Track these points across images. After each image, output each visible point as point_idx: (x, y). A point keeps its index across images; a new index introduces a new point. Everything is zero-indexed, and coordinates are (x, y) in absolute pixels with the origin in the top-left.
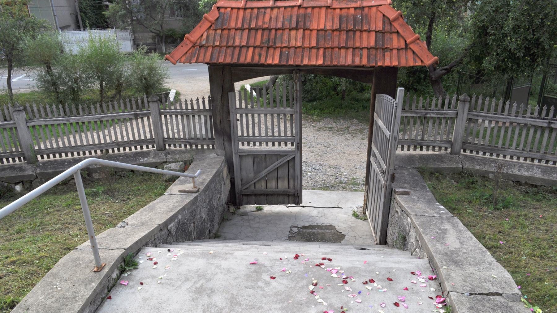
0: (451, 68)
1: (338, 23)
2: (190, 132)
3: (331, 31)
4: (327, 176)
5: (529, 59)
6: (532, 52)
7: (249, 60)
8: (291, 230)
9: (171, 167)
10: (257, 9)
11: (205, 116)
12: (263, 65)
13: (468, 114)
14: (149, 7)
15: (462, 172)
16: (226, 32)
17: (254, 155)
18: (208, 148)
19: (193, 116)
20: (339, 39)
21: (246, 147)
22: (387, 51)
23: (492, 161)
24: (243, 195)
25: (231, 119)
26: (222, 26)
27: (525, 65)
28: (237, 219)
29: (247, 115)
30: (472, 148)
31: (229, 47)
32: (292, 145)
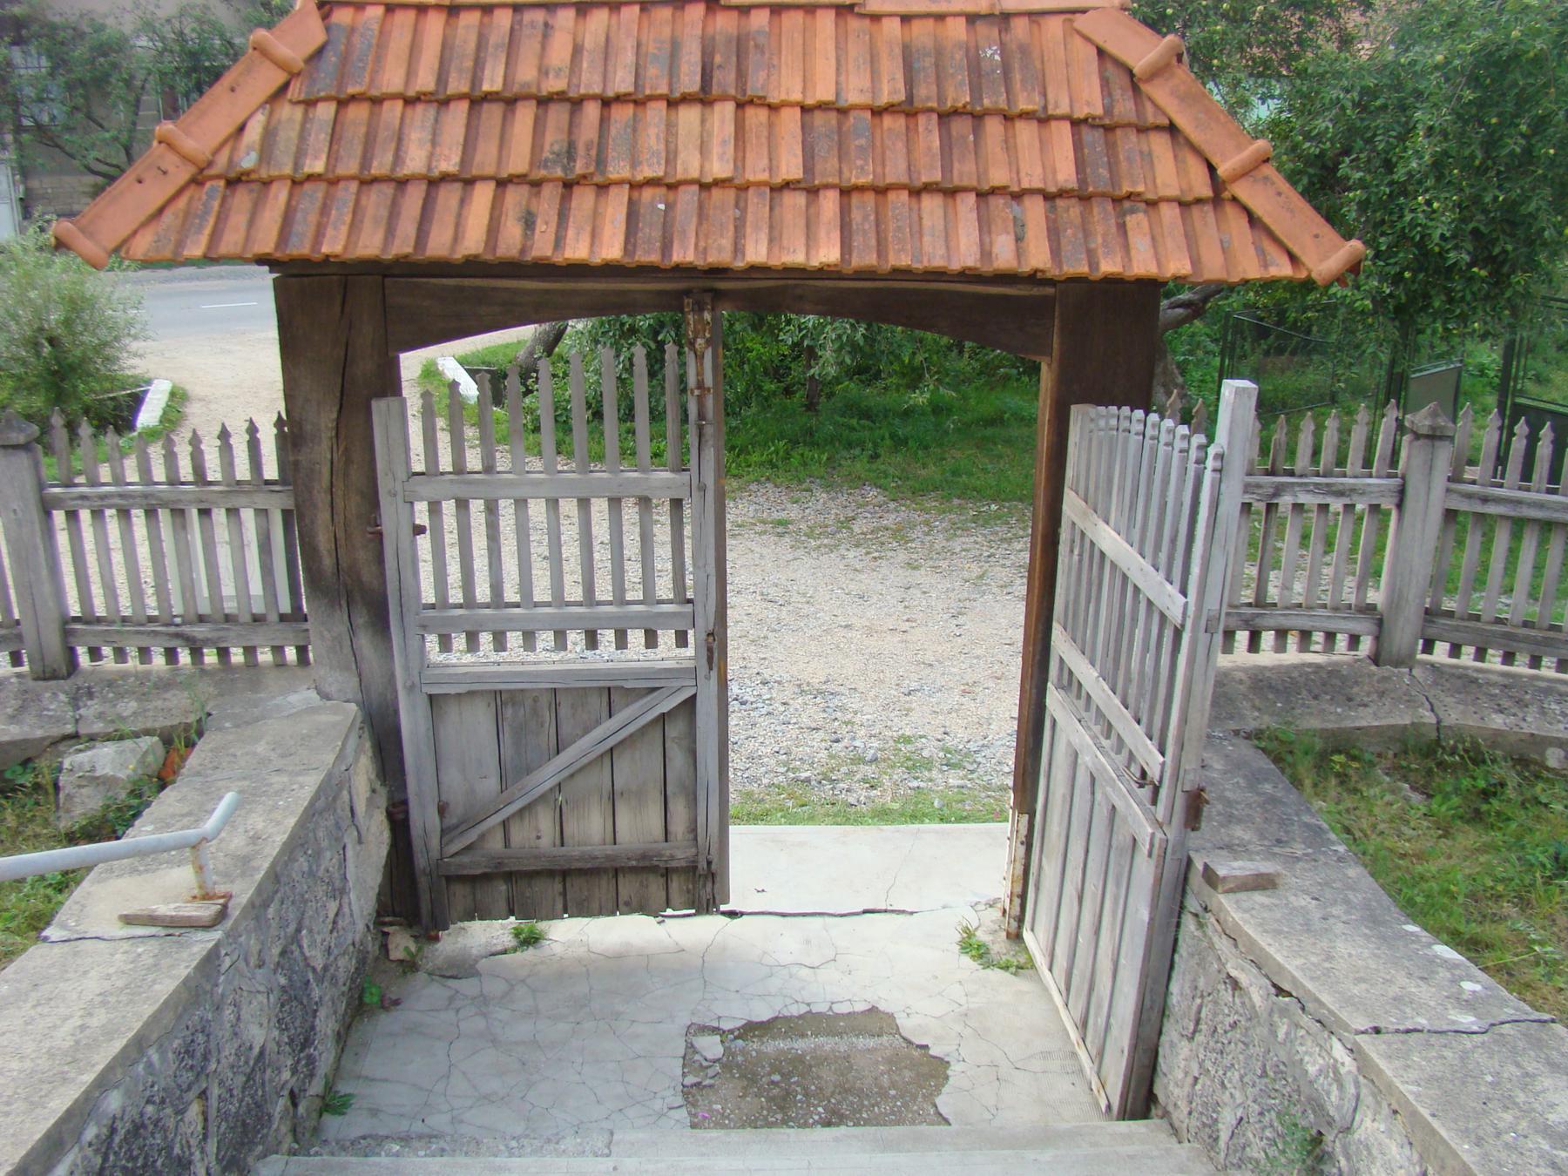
0: (1205, 300)
1: (900, 76)
2: (188, 589)
3: (868, 115)
4: (793, 732)
5: (1483, 273)
6: (1496, 251)
7: (473, 243)
8: (690, 1046)
9: (93, 769)
10: (510, 12)
11: (262, 513)
12: (544, 269)
13: (1448, 490)
14: (81, 82)
15: (1438, 741)
16: (358, 113)
17: (497, 694)
18: (280, 664)
19: (205, 513)
20: (909, 152)
21: (459, 657)
22: (1132, 212)
23: (1547, 692)
24: (450, 879)
25: (387, 526)
26: (341, 85)
27: (1473, 294)
28: (424, 995)
29: (462, 505)
30: (1457, 637)
31: (375, 180)
32: (682, 640)
